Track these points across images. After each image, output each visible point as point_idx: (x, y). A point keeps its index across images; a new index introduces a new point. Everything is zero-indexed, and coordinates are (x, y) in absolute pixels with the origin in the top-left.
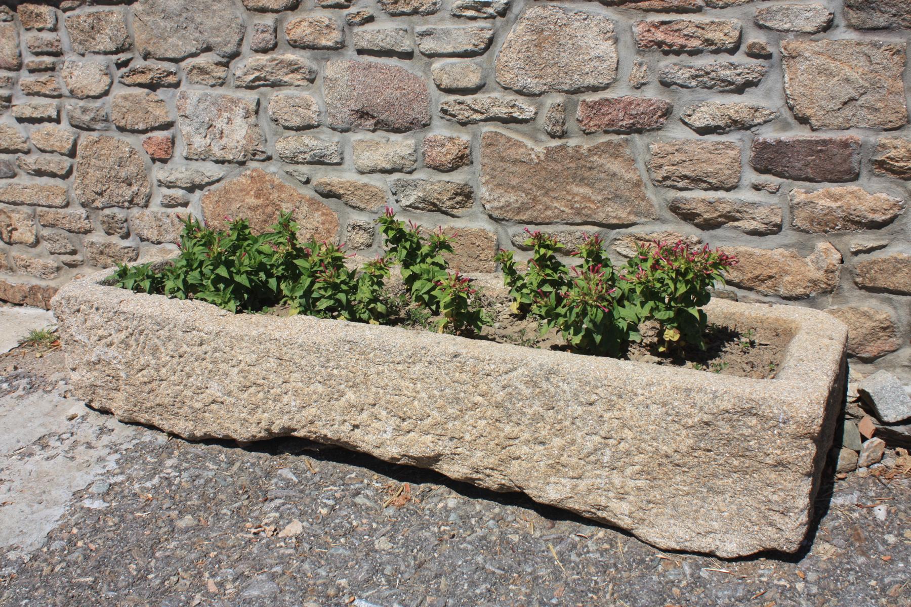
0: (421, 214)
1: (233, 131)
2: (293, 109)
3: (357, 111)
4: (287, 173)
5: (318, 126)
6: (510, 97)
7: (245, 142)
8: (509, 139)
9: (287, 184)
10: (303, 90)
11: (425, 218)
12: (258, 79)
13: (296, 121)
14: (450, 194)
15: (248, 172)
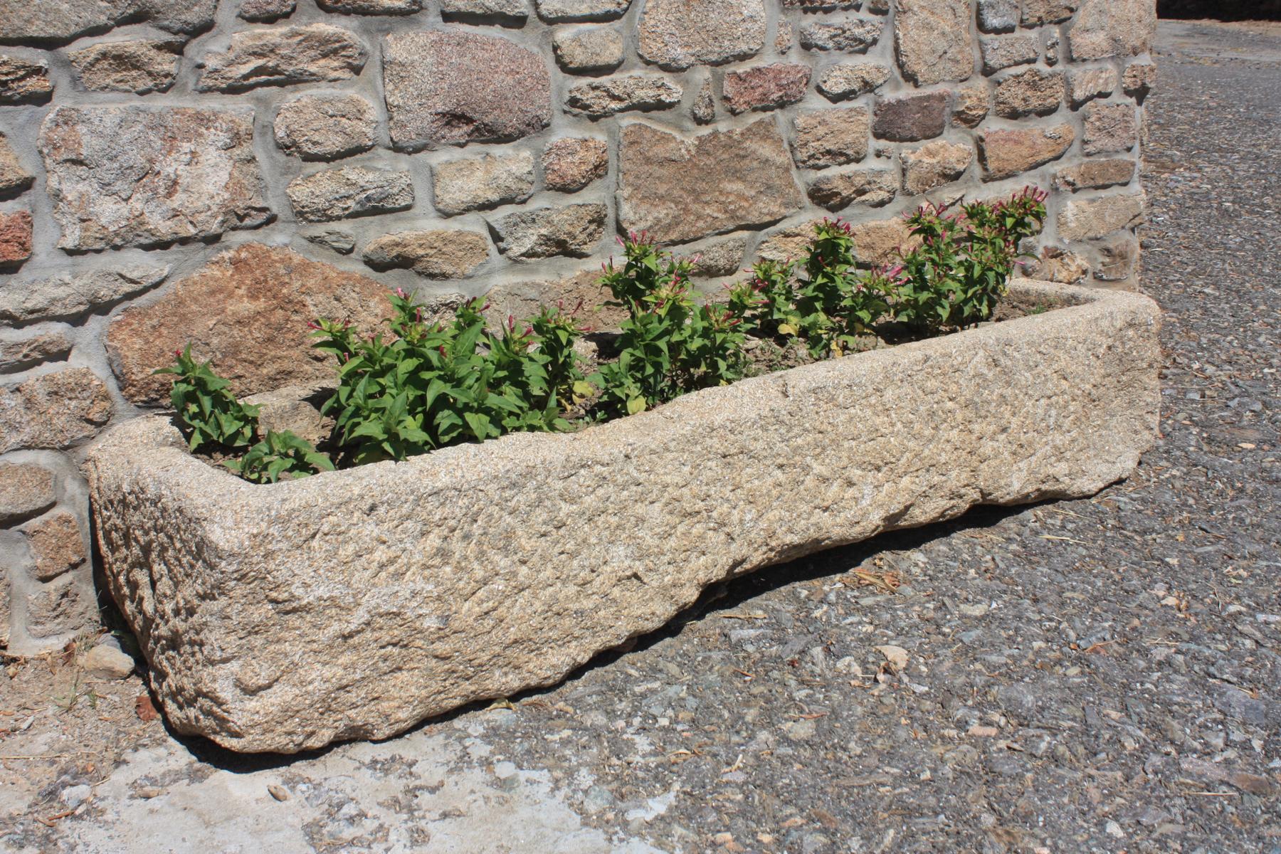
0: (538, 263)
1: (199, 176)
2: (331, 121)
3: (444, 115)
4: (312, 240)
5: (371, 148)
6: (656, 75)
7: (227, 195)
8: (655, 132)
9: (314, 260)
10: (345, 87)
11: (543, 268)
12: (258, 71)
13: (334, 143)
14: (584, 223)
15: (227, 255)
